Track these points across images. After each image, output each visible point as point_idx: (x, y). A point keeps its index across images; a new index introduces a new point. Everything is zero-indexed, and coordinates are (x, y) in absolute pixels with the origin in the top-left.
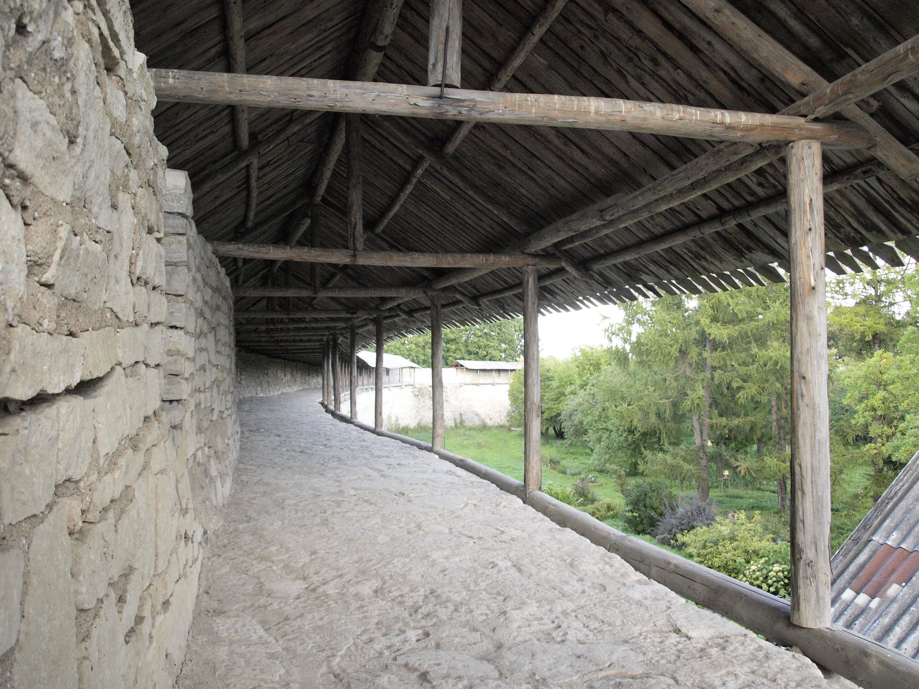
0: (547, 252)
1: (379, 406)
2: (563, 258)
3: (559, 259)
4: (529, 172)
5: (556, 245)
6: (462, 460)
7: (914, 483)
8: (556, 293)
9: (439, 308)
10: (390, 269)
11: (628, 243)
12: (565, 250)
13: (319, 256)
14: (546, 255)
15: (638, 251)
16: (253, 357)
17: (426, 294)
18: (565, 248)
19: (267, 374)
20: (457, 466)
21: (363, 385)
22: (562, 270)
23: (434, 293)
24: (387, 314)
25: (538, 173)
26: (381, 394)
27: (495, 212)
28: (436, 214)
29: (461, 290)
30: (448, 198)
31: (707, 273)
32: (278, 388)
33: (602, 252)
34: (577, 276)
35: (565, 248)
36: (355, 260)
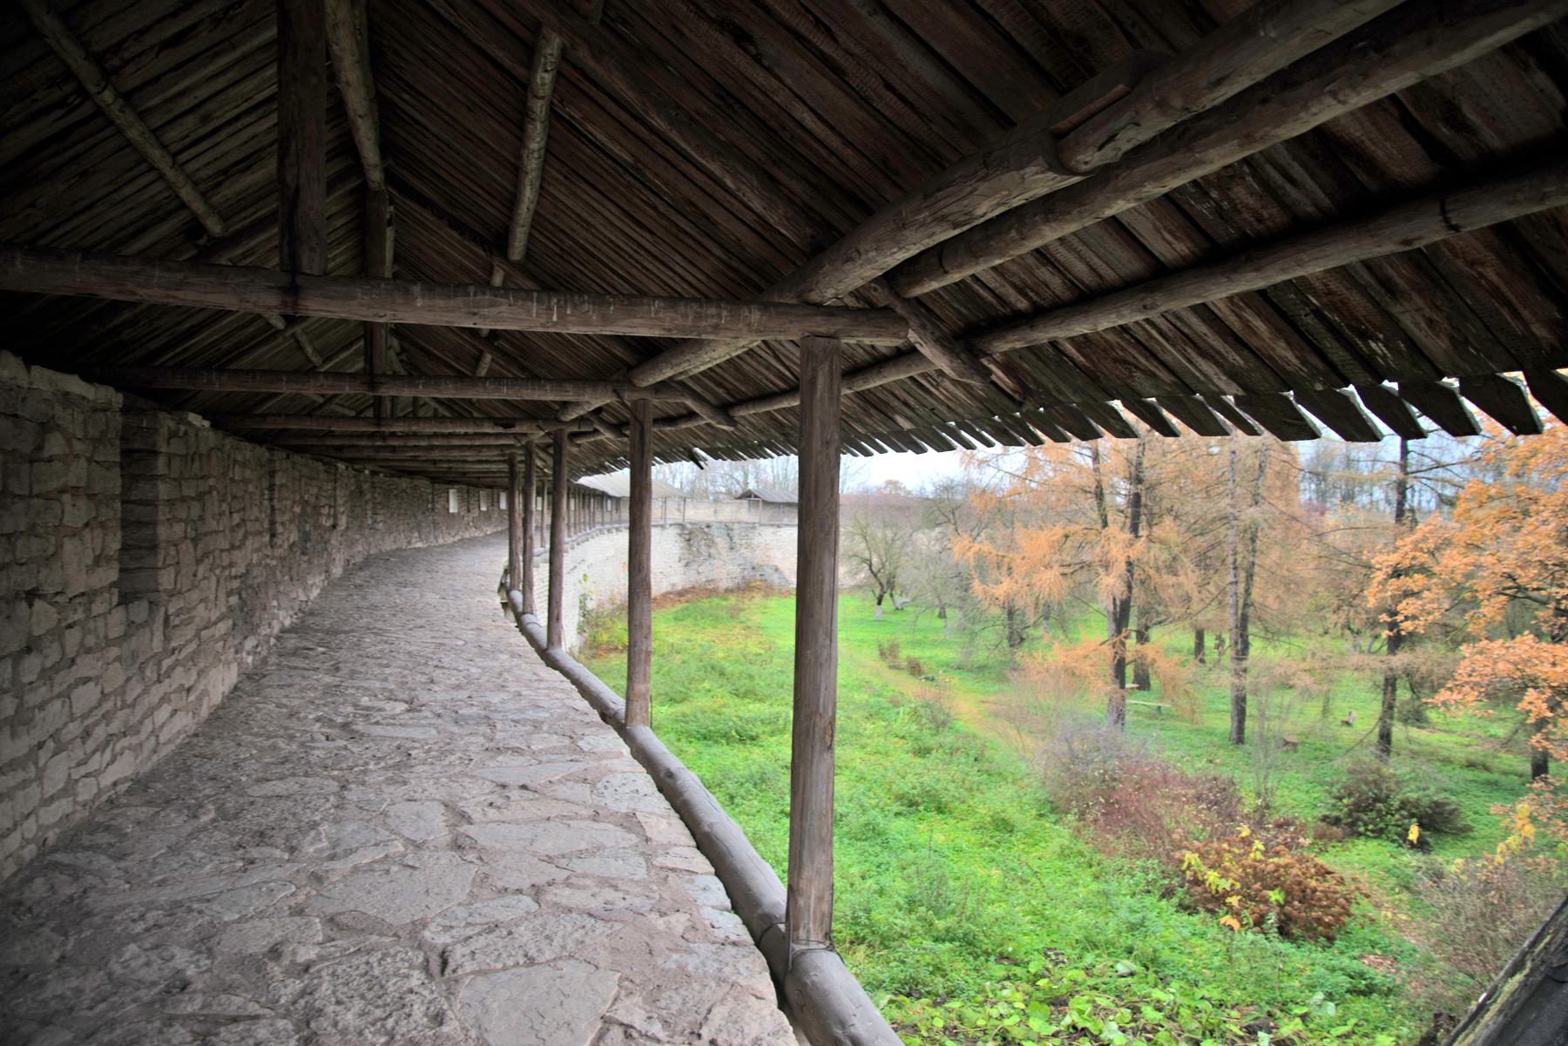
0: (870, 303)
1: (554, 604)
2: (913, 322)
3: (902, 321)
4: (820, 41)
5: (893, 279)
6: (670, 775)
7: (427, 7)
8: (893, 409)
9: (647, 426)
10: (560, 340)
11: (1110, 275)
12: (917, 299)
13: (180, 286)
14: (866, 309)
15: (1148, 302)
16: (404, 483)
17: (619, 397)
18: (918, 291)
19: (433, 509)
20: (660, 790)
21: (603, 524)
22: (907, 354)
23: (636, 396)
24: (575, 429)
25: (842, 37)
26: (561, 582)
27: (729, 182)
28: (613, 208)
29: (699, 389)
30: (630, 160)
31: (1367, 379)
32: (453, 533)
33: (1022, 304)
34: (947, 370)
35: (918, 291)
36: (295, 305)
